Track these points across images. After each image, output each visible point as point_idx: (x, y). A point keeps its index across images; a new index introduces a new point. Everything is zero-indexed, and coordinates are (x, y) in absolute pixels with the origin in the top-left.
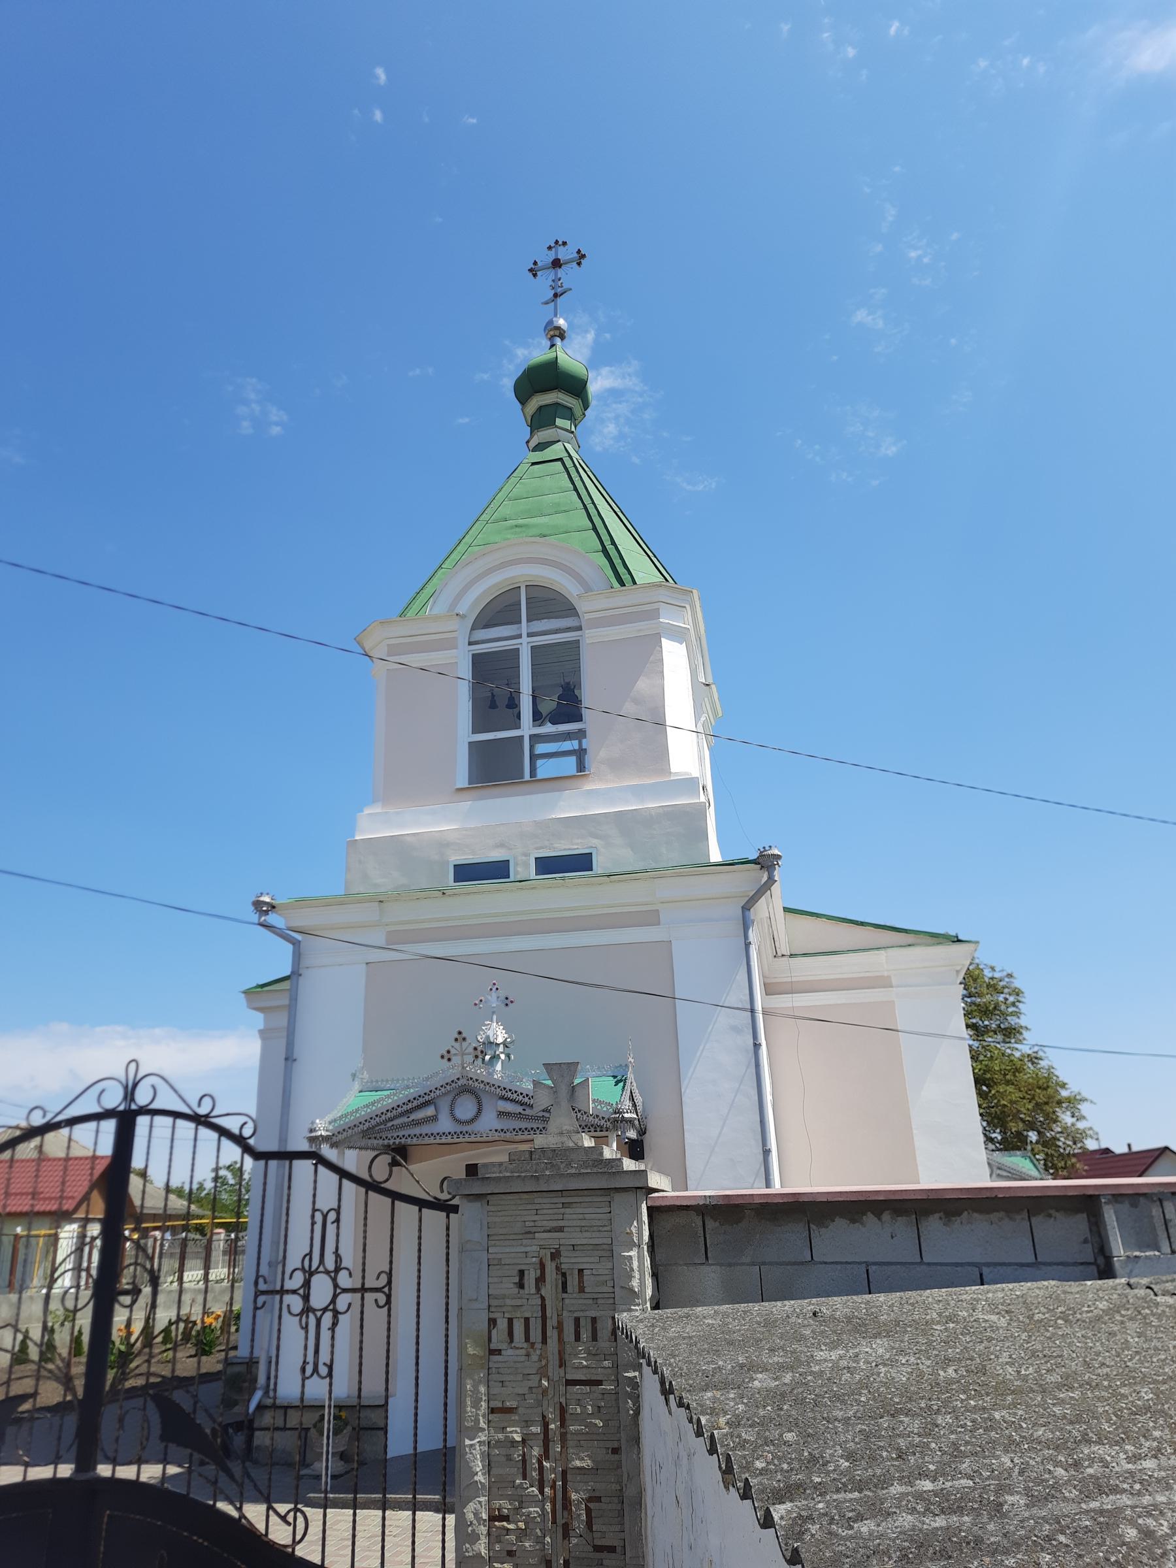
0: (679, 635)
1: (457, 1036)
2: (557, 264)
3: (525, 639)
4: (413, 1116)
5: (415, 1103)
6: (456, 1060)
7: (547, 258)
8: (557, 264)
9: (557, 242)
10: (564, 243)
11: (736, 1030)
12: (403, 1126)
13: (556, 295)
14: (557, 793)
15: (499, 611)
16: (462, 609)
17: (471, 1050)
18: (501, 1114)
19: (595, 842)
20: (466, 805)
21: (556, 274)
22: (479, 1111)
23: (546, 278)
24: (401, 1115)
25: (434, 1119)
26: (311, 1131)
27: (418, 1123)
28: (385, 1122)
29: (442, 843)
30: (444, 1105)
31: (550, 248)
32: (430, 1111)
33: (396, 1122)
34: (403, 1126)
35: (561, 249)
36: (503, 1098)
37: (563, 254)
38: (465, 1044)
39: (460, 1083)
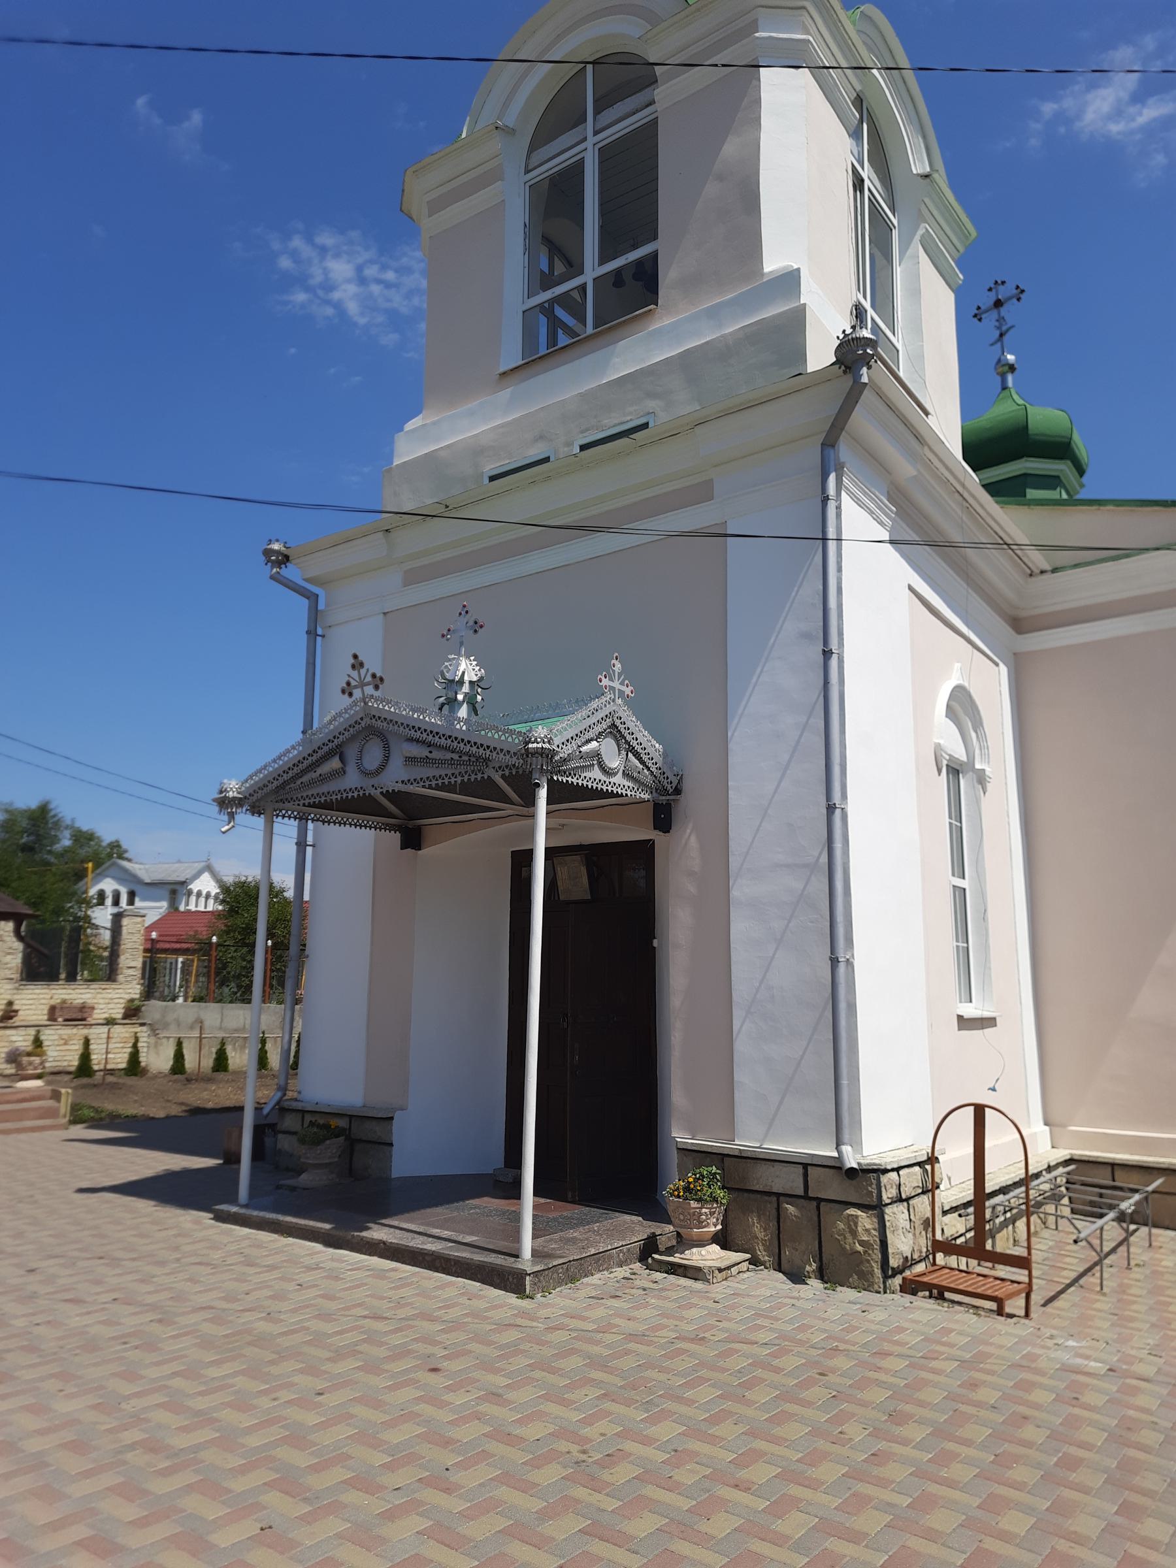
0: (793, 58)
1: (352, 661)
2: (998, 304)
3: (589, 144)
4: (320, 771)
5: (320, 753)
6: (357, 693)
7: (988, 300)
8: (998, 304)
9: (996, 282)
10: (1003, 283)
11: (807, 636)
12: (312, 783)
13: (1001, 335)
14: (611, 347)
15: (560, 116)
16: (510, 120)
17: (369, 678)
18: (410, 760)
19: (652, 405)
20: (506, 394)
21: (999, 313)
22: (387, 758)
23: (990, 319)
24: (304, 772)
25: (342, 772)
26: (221, 792)
27: (323, 779)
28: (293, 779)
29: (476, 451)
30: (351, 753)
31: (990, 289)
32: (335, 763)
33: (305, 779)
34: (312, 783)
35: (1001, 288)
36: (411, 740)
37: (1003, 293)
38: (363, 671)
39: (363, 724)
